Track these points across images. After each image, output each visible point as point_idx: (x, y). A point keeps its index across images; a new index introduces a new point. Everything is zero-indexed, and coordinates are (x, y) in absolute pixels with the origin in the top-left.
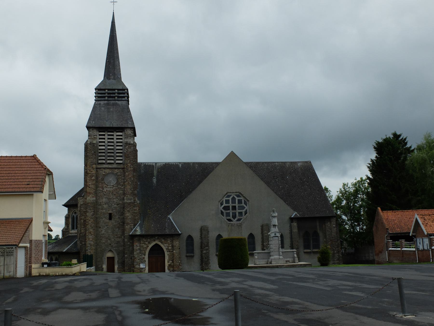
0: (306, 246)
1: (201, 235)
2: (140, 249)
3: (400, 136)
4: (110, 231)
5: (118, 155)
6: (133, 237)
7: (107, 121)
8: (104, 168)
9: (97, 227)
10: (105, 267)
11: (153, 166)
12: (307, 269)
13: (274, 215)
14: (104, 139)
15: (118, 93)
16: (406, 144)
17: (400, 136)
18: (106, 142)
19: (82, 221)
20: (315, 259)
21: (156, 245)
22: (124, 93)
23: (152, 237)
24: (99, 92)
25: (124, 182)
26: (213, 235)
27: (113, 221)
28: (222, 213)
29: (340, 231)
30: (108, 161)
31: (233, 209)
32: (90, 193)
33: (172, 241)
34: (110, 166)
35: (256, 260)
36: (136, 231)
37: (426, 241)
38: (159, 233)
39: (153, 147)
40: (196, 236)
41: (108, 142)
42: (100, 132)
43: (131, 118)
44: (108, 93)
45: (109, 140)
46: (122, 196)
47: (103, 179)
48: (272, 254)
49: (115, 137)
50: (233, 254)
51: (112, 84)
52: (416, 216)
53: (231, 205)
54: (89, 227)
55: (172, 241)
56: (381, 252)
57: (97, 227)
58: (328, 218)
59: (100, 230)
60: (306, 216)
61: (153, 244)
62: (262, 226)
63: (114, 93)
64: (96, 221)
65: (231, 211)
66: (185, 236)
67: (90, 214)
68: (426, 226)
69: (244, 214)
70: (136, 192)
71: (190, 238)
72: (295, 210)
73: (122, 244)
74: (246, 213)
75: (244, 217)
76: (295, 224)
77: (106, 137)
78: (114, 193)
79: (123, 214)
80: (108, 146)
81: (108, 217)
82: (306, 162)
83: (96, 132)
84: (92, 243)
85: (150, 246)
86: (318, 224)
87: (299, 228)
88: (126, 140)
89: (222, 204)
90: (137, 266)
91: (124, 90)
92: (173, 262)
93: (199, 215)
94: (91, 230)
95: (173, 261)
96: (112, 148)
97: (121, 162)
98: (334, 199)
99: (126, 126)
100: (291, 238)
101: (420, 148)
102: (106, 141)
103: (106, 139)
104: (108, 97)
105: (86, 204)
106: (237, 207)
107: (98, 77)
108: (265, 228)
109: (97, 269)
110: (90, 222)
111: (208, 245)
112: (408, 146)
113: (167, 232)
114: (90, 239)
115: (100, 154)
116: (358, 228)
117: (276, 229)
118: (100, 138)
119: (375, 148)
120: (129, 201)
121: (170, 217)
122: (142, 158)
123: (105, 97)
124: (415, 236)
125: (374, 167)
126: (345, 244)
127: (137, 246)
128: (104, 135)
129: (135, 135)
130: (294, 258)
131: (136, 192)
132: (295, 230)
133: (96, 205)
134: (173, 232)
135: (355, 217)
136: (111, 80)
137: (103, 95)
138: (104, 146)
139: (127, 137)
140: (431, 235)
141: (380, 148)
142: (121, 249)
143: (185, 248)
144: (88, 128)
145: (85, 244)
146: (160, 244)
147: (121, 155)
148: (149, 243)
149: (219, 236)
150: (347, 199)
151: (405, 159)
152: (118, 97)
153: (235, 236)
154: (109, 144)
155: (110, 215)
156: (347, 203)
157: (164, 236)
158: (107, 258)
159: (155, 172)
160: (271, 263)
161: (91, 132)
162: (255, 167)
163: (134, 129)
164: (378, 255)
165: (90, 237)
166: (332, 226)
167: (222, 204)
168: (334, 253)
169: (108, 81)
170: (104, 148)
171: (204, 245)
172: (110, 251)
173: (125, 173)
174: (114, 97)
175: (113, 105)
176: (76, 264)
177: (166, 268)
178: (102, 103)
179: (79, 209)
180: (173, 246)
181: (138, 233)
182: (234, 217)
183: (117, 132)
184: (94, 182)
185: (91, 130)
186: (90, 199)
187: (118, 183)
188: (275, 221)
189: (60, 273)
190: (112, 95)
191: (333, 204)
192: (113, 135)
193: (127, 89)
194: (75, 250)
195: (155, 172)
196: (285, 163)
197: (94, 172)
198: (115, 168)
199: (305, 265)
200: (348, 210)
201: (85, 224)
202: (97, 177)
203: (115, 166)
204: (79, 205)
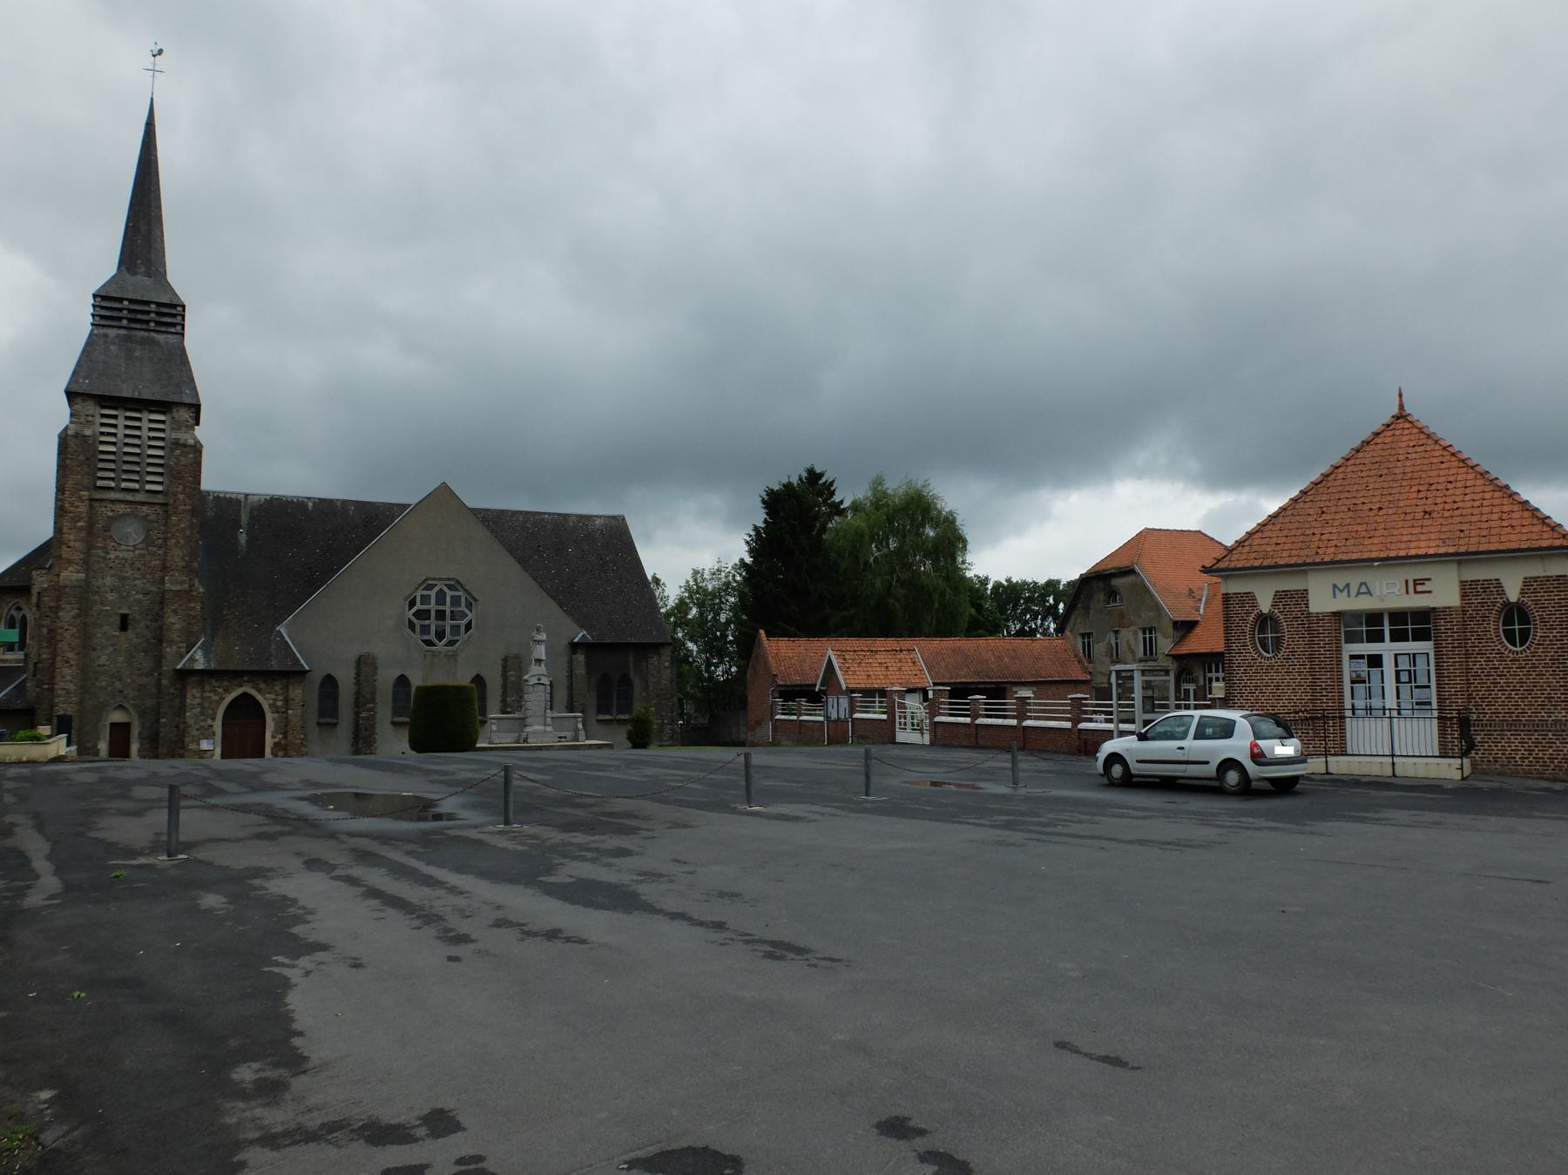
0: (603, 708)
1: (358, 674)
2: (200, 705)
3: (821, 475)
4: (121, 659)
5: (150, 469)
6: (184, 675)
7: (124, 381)
8: (113, 501)
9: (86, 644)
10: (103, 746)
11: (238, 502)
12: (606, 752)
13: (539, 637)
14: (115, 426)
15: (157, 313)
16: (833, 493)
17: (821, 475)
18: (120, 435)
19: (45, 631)
20: (621, 735)
21: (245, 695)
22: (174, 316)
23: (235, 675)
24: (104, 304)
25: (166, 540)
26: (386, 677)
27: (130, 633)
28: (412, 626)
29: (680, 675)
30: (124, 485)
31: (435, 619)
32: (70, 562)
33: (286, 688)
34: (129, 497)
35: (495, 733)
36: (192, 660)
37: (844, 702)
38: (254, 668)
39: (241, 457)
40: (346, 678)
41: (126, 436)
42: (103, 407)
43: (192, 380)
44: (130, 311)
45: (128, 432)
46: (159, 574)
47: (107, 529)
48: (529, 721)
49: (145, 425)
50: (443, 721)
51: (139, 287)
52: (830, 652)
53: (433, 606)
54: (63, 646)
55: (286, 688)
56: (759, 723)
57: (86, 644)
58: (656, 647)
59: (93, 654)
60: (608, 640)
61: (239, 691)
62: (505, 660)
63: (148, 313)
64: (86, 634)
65: (433, 624)
66: (317, 677)
67: (68, 614)
68: (846, 671)
69: (463, 629)
70: (196, 564)
71: (330, 682)
72: (582, 627)
73: (154, 690)
74: (468, 627)
75: (463, 636)
76: (581, 657)
77: (121, 422)
78: (138, 564)
79: (158, 617)
80: (127, 444)
81: (117, 621)
82: (614, 518)
83: (91, 408)
84: (72, 687)
85: (229, 698)
86: (631, 659)
87: (590, 667)
88: (174, 435)
89: (412, 603)
90: (192, 746)
91: (174, 306)
92: (285, 737)
93: (352, 628)
94: (71, 655)
95: (285, 734)
96: (137, 450)
97: (159, 488)
98: (671, 603)
99: (175, 399)
100: (571, 687)
101: (856, 507)
102: (121, 432)
103: (121, 427)
104: (130, 320)
105: (59, 591)
106: (448, 613)
107: (99, 257)
108: (513, 666)
109: (80, 752)
110: (69, 635)
111: (373, 701)
112: (837, 498)
113: (274, 665)
114: (67, 679)
115: (101, 465)
116: (719, 671)
117: (542, 669)
118: (103, 425)
119: (764, 501)
120: (178, 587)
121: (282, 629)
122: (211, 481)
123: (120, 319)
124: (824, 692)
125: (762, 544)
126: (689, 708)
127: (193, 696)
128: (115, 417)
129: (198, 424)
130: (576, 730)
131: (196, 564)
132: (580, 671)
133: (84, 594)
134: (288, 666)
135: (715, 648)
136: (139, 277)
137: (115, 314)
138: (114, 444)
139: (177, 426)
140: (853, 691)
141: (775, 502)
142: (150, 702)
143: (316, 705)
144: (71, 395)
145: (52, 690)
146: (254, 693)
147: (160, 470)
148: (227, 691)
149: (402, 681)
150: (700, 605)
151: (823, 529)
152: (158, 323)
153: (439, 679)
154: (128, 440)
155: (124, 618)
156: (701, 613)
157: (266, 676)
158: (112, 724)
159: (244, 518)
160: (525, 741)
161: (77, 407)
162: (494, 521)
163: (196, 408)
164: (752, 729)
165: (67, 671)
166: (661, 669)
167: (412, 603)
168: (662, 724)
169: (130, 280)
170: (113, 449)
171: (363, 700)
172: (121, 707)
173: (167, 516)
174: (147, 322)
175: (144, 342)
176: (49, 737)
177: (268, 750)
178: (112, 332)
179: (34, 599)
180: (286, 700)
181: (200, 666)
182: (440, 635)
183: (151, 412)
184: (83, 534)
185: (78, 400)
186: (71, 575)
187: (148, 541)
188: (541, 651)
189: (14, 758)
190: (139, 316)
191: (668, 615)
192: (139, 419)
193: (184, 307)
194: (19, 704)
195: (244, 518)
196: (566, 516)
197: (83, 508)
198: (143, 504)
199: (599, 747)
200: (700, 629)
201: (52, 638)
202: (91, 524)
203: (140, 497)
204: (35, 590)
